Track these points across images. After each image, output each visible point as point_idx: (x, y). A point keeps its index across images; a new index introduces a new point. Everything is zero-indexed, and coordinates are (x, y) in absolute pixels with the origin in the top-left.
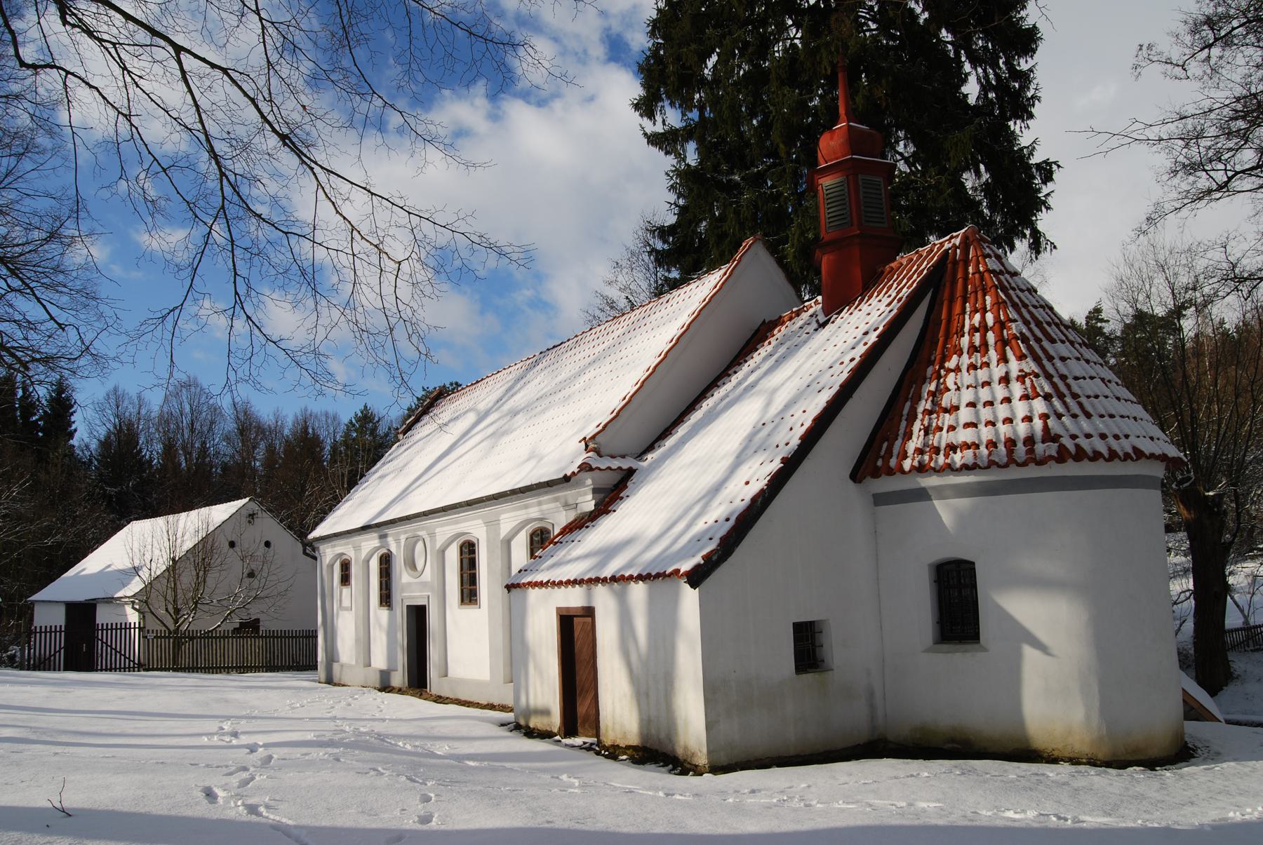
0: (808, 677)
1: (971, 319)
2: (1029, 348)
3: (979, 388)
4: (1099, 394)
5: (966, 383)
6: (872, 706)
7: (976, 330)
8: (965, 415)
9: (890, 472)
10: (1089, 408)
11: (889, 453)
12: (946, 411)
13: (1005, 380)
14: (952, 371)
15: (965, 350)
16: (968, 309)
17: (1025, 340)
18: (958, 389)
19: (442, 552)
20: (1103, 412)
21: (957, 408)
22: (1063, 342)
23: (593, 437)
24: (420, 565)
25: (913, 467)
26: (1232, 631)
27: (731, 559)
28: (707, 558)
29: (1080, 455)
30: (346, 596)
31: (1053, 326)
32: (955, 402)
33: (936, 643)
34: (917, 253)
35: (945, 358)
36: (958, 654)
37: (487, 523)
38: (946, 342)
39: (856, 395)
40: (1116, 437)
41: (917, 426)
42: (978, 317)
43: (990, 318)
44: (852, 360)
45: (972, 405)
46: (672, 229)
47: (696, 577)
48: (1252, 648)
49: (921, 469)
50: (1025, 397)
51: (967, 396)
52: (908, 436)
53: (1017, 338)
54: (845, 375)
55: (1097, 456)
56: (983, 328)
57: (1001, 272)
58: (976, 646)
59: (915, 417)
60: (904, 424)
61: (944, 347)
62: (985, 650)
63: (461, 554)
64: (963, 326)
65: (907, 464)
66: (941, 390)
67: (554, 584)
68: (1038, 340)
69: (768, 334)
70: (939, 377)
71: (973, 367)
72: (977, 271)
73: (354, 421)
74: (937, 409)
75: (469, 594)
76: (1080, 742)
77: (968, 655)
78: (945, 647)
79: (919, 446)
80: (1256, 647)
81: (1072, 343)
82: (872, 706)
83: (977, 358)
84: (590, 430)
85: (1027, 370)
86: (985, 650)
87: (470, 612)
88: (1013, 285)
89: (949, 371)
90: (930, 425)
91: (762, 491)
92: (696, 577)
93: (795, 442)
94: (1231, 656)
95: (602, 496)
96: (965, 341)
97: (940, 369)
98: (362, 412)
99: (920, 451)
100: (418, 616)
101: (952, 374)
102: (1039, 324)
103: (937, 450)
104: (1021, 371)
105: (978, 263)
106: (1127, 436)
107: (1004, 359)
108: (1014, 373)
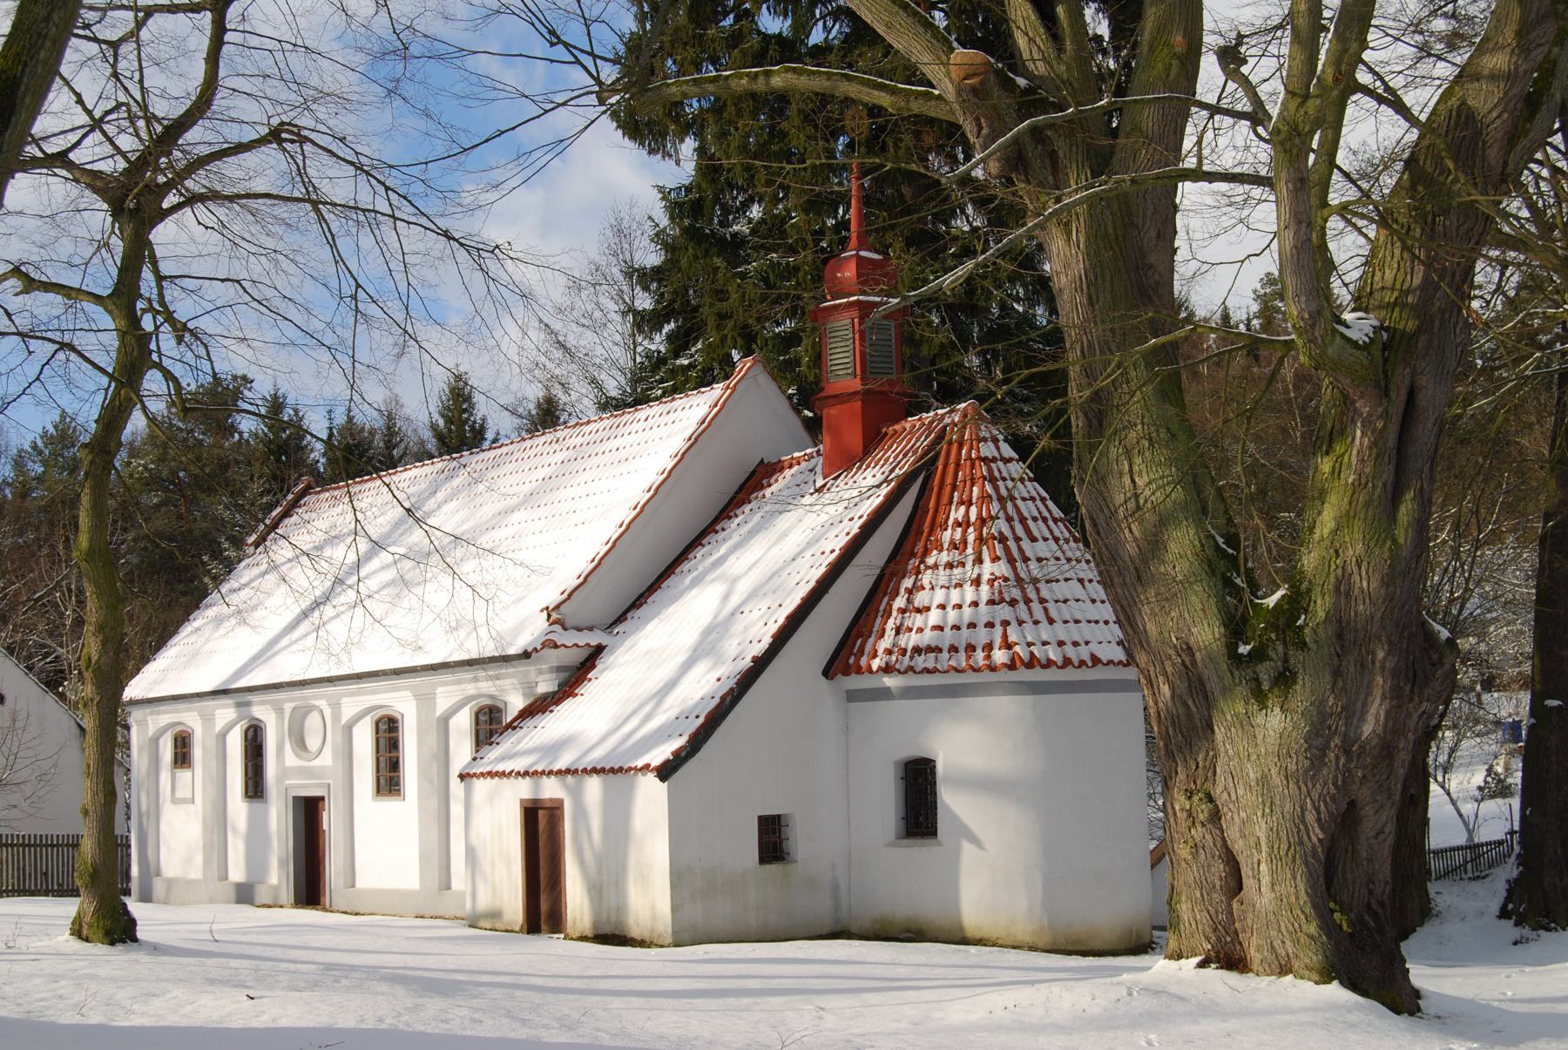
0: (772, 868)
1: (956, 510)
2: (1007, 550)
3: (952, 589)
4: (1069, 597)
5: (941, 583)
6: (836, 898)
7: (959, 525)
8: (934, 617)
9: (859, 671)
10: (1053, 614)
11: (861, 651)
12: (918, 611)
13: (977, 582)
14: (930, 567)
15: (946, 546)
16: (955, 499)
17: (1002, 539)
18: (932, 588)
19: (349, 728)
20: (1068, 618)
21: (928, 609)
22: (1045, 539)
23: (557, 607)
24: (313, 742)
25: (880, 668)
26: (1436, 852)
27: (698, 755)
28: (676, 754)
29: (1032, 663)
30: (193, 781)
31: (1040, 522)
32: (926, 603)
33: (899, 838)
34: (920, 419)
35: (926, 553)
36: (916, 849)
37: (418, 697)
38: (930, 534)
39: (832, 591)
40: (1075, 644)
41: (891, 624)
42: (962, 509)
43: (973, 511)
44: (833, 551)
45: (942, 607)
46: (657, 273)
47: (665, 771)
48: (1470, 875)
49: (887, 669)
50: (991, 602)
51: (939, 595)
52: (882, 635)
53: (995, 538)
54: (823, 570)
55: (1049, 664)
56: (964, 524)
57: (994, 460)
58: (933, 841)
59: (890, 615)
60: (879, 620)
61: (928, 540)
62: (940, 844)
63: (377, 732)
64: (948, 518)
65: (875, 664)
66: (917, 588)
67: (503, 774)
68: (1018, 539)
69: (765, 482)
70: (918, 573)
71: (950, 566)
72: (969, 458)
73: (40, 443)
74: (910, 609)
75: (389, 780)
76: (1023, 932)
77: (925, 849)
78: (906, 841)
79: (888, 646)
80: (1476, 874)
81: (1056, 540)
82: (836, 898)
83: (955, 556)
84: (552, 597)
85: (998, 574)
86: (940, 844)
87: (389, 805)
88: (1005, 474)
89: (928, 567)
90: (902, 624)
91: (732, 689)
92: (665, 771)
93: (767, 640)
94: (1432, 888)
95: (566, 675)
96: (947, 536)
97: (921, 562)
98: (56, 427)
99: (889, 652)
100: (309, 811)
101: (929, 571)
102: (1023, 520)
103: (904, 652)
104: (992, 574)
105: (971, 448)
106: (1087, 643)
107: (979, 560)
108: (986, 577)
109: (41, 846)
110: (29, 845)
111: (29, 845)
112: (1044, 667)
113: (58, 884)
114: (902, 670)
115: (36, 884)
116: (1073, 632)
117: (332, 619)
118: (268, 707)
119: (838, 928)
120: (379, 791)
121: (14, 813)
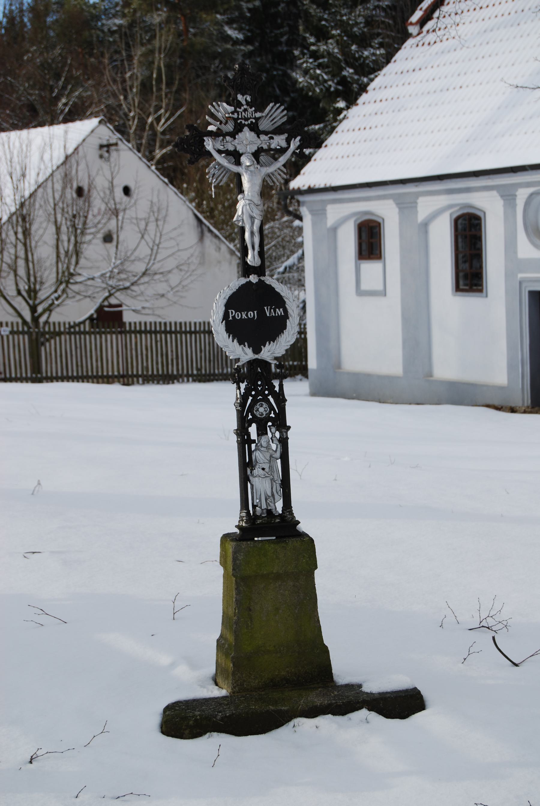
109: (181, 332)
110: (171, 332)
111: (171, 332)
113: (198, 369)
115: (178, 370)
117: (136, 214)
118: (494, 193)
120: (459, 288)
121: (162, 302)
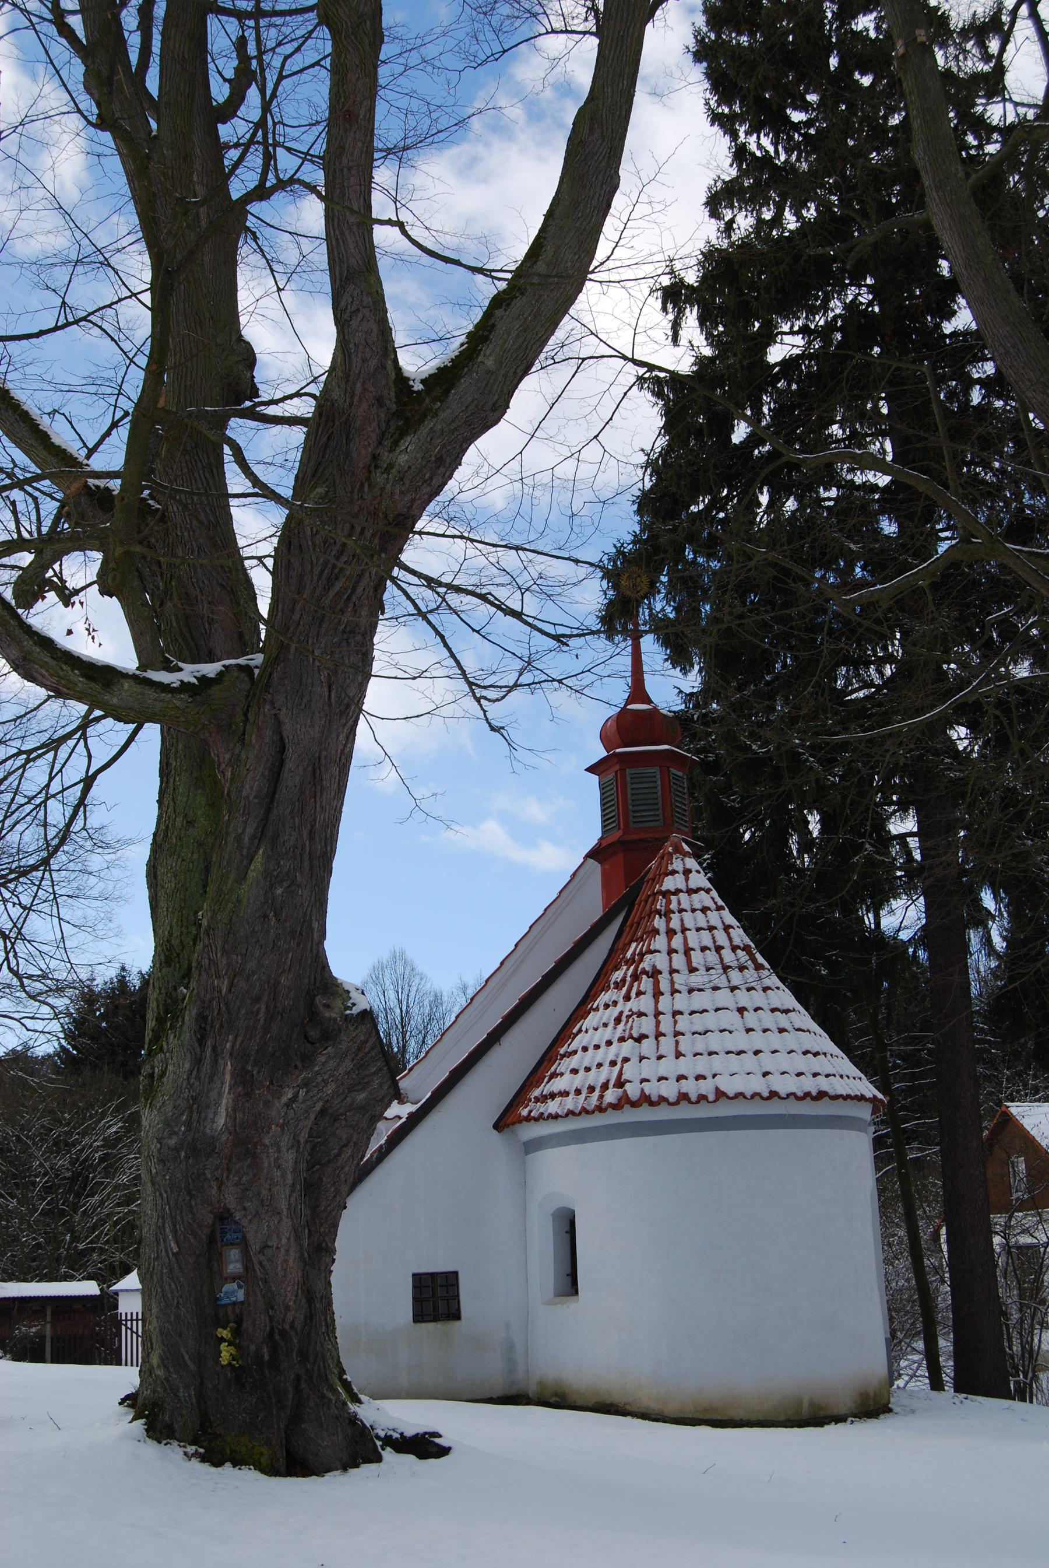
6: (510, 1361)
112: (652, 1104)
114: (577, 1112)
116: (702, 1065)
119: (513, 1391)
